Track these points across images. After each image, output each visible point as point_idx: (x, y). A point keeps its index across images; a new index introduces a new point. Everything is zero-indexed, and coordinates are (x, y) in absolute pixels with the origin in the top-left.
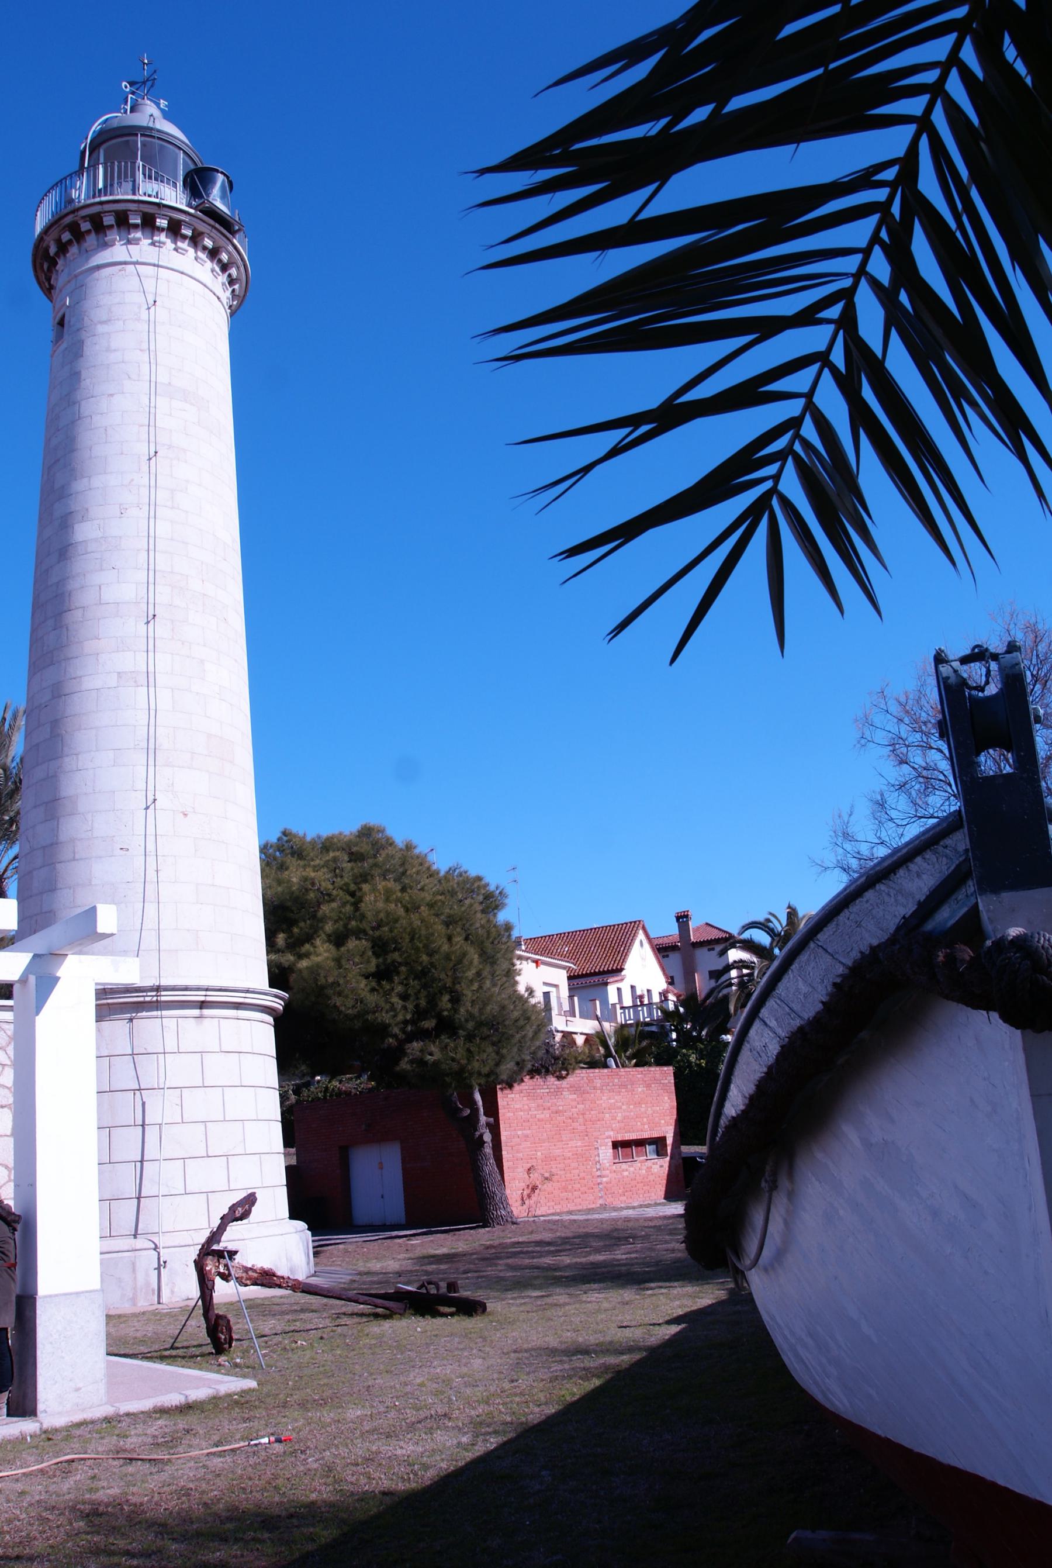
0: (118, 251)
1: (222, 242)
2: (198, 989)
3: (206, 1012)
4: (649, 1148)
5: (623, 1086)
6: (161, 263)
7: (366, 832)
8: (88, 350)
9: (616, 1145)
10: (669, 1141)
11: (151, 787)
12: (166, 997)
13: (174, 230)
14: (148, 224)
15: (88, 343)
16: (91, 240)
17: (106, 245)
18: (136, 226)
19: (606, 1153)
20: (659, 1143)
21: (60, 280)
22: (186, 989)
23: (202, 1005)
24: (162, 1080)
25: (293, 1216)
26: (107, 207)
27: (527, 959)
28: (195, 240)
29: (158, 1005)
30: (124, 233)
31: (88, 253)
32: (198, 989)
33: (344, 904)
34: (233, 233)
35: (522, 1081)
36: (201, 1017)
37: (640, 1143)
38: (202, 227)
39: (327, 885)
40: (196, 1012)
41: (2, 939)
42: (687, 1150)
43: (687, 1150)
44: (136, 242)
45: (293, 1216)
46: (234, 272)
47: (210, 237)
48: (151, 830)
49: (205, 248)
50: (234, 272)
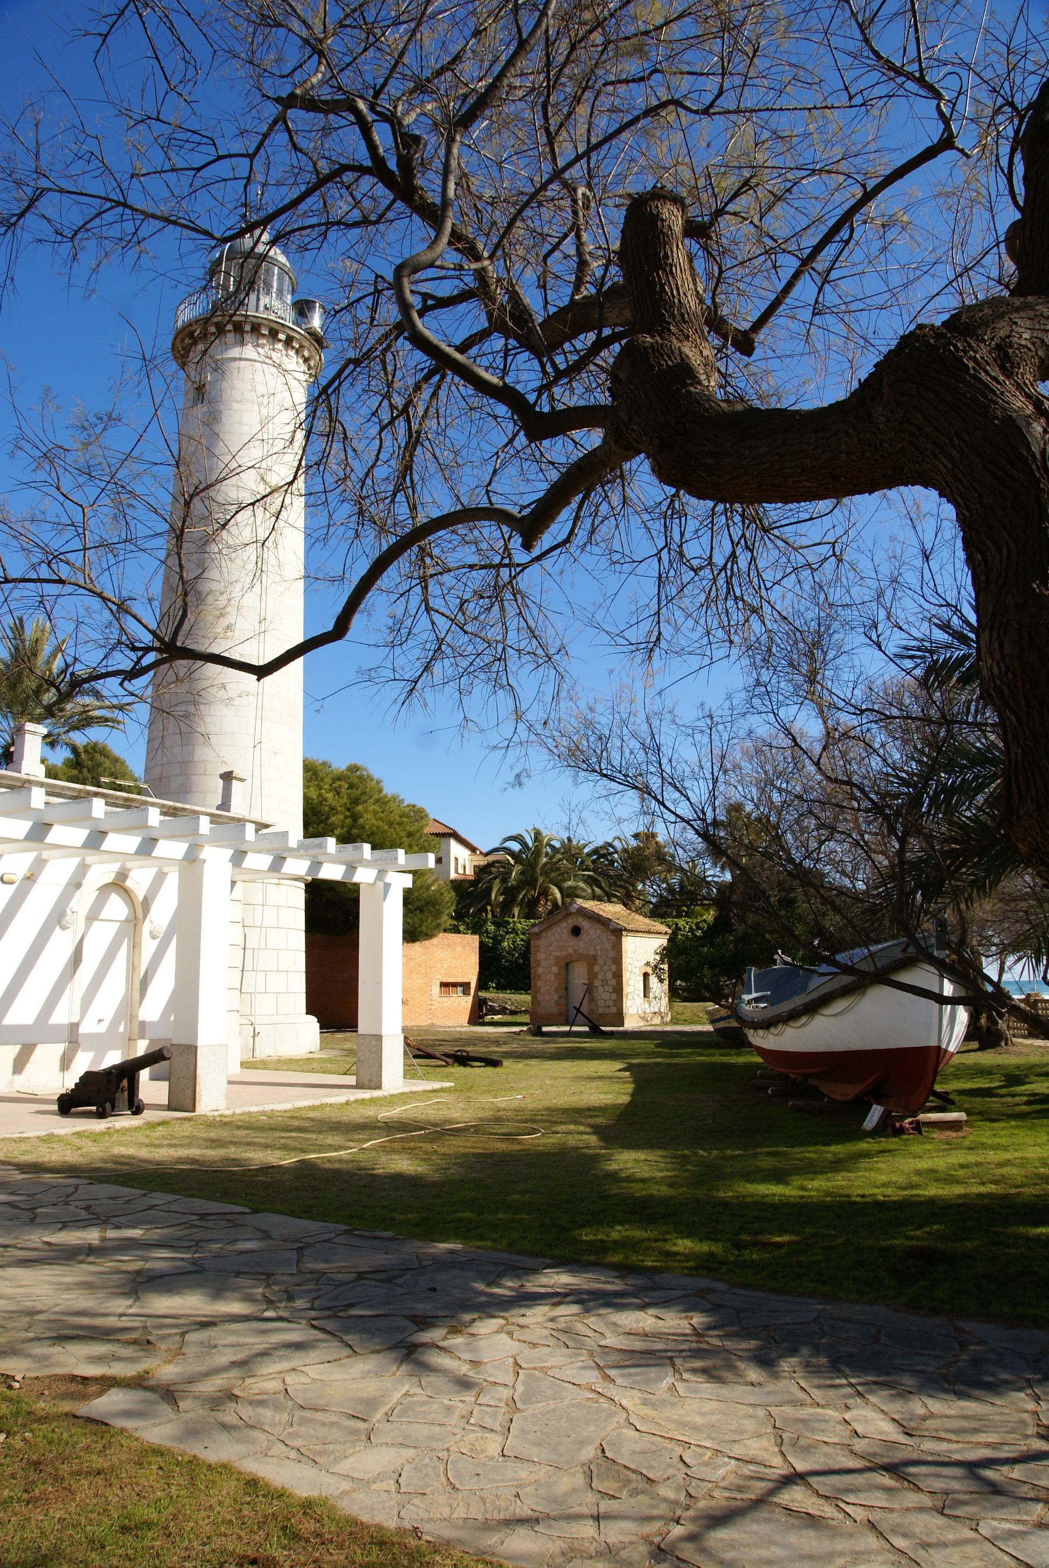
0: (249, 351)
4: (460, 989)
5: (449, 945)
6: (536, 565)
7: (354, 769)
8: (225, 418)
9: (444, 985)
10: (473, 986)
11: (258, 733)
13: (288, 342)
14: (273, 334)
15: (225, 414)
16: (230, 337)
17: (242, 343)
18: (264, 335)
19: (436, 989)
20: (466, 986)
21: (194, 356)
25: (308, 1012)
30: (254, 338)
31: (227, 347)
33: (346, 817)
34: (322, 348)
37: (454, 985)
38: (306, 344)
39: (334, 804)
41: (1043, 1114)
42: (482, 994)
43: (482, 994)
44: (263, 346)
45: (308, 1012)
48: (257, 762)
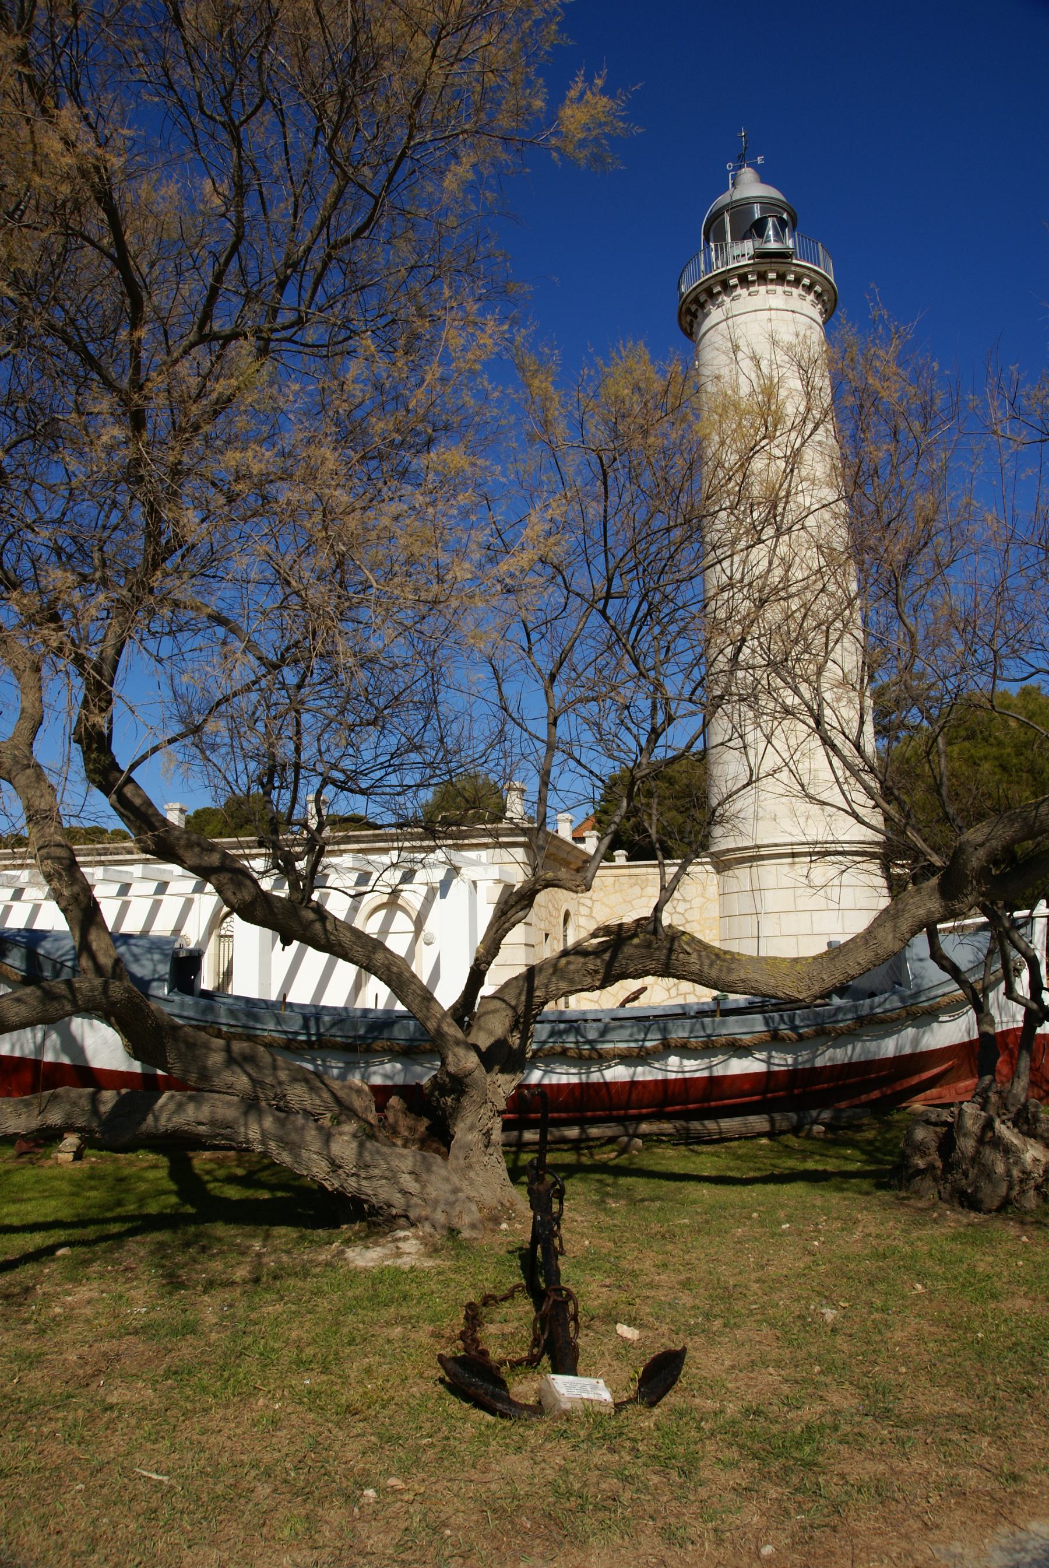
1: (782, 268)
2: (785, 845)
3: (797, 860)
12: (764, 852)
13: (744, 281)
18: (719, 293)
22: (776, 845)
23: (793, 855)
24: (759, 907)
26: (699, 290)
27: (345, 851)
28: (762, 278)
29: (763, 858)
32: (785, 845)
35: (670, 926)
36: (793, 863)
38: (762, 268)
40: (790, 860)
46: (818, 288)
47: (772, 271)
49: (772, 280)
50: (818, 288)
